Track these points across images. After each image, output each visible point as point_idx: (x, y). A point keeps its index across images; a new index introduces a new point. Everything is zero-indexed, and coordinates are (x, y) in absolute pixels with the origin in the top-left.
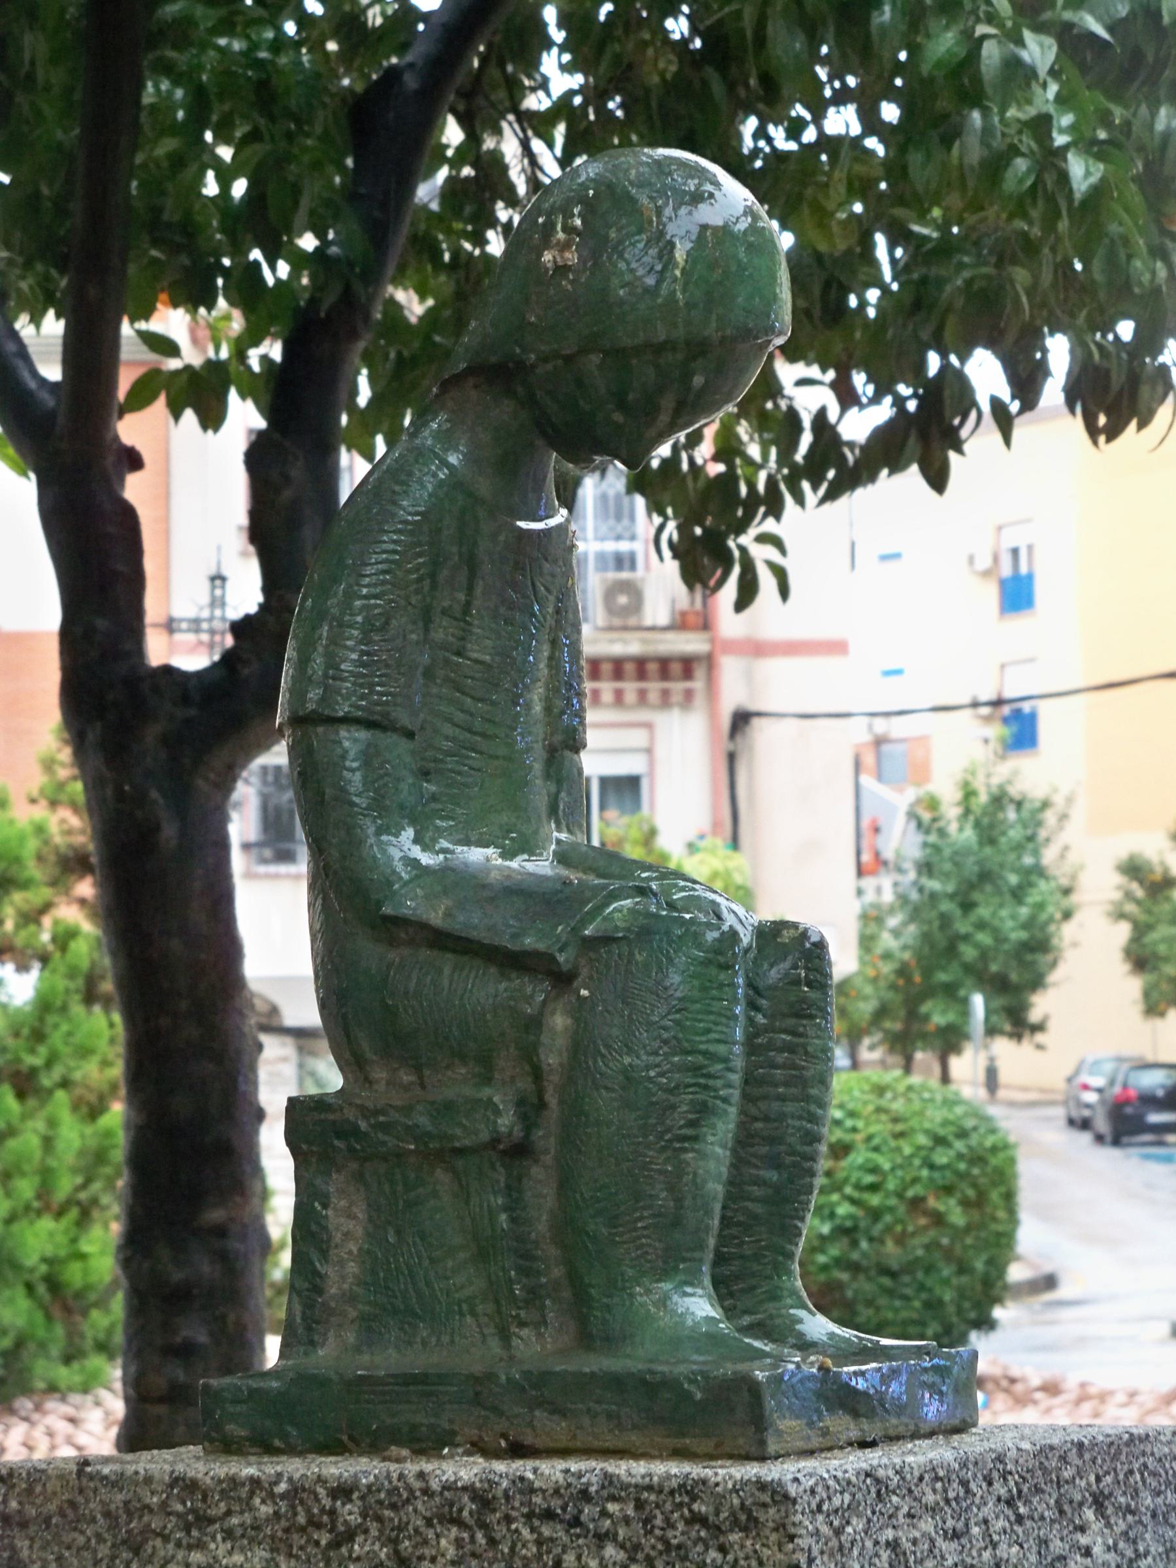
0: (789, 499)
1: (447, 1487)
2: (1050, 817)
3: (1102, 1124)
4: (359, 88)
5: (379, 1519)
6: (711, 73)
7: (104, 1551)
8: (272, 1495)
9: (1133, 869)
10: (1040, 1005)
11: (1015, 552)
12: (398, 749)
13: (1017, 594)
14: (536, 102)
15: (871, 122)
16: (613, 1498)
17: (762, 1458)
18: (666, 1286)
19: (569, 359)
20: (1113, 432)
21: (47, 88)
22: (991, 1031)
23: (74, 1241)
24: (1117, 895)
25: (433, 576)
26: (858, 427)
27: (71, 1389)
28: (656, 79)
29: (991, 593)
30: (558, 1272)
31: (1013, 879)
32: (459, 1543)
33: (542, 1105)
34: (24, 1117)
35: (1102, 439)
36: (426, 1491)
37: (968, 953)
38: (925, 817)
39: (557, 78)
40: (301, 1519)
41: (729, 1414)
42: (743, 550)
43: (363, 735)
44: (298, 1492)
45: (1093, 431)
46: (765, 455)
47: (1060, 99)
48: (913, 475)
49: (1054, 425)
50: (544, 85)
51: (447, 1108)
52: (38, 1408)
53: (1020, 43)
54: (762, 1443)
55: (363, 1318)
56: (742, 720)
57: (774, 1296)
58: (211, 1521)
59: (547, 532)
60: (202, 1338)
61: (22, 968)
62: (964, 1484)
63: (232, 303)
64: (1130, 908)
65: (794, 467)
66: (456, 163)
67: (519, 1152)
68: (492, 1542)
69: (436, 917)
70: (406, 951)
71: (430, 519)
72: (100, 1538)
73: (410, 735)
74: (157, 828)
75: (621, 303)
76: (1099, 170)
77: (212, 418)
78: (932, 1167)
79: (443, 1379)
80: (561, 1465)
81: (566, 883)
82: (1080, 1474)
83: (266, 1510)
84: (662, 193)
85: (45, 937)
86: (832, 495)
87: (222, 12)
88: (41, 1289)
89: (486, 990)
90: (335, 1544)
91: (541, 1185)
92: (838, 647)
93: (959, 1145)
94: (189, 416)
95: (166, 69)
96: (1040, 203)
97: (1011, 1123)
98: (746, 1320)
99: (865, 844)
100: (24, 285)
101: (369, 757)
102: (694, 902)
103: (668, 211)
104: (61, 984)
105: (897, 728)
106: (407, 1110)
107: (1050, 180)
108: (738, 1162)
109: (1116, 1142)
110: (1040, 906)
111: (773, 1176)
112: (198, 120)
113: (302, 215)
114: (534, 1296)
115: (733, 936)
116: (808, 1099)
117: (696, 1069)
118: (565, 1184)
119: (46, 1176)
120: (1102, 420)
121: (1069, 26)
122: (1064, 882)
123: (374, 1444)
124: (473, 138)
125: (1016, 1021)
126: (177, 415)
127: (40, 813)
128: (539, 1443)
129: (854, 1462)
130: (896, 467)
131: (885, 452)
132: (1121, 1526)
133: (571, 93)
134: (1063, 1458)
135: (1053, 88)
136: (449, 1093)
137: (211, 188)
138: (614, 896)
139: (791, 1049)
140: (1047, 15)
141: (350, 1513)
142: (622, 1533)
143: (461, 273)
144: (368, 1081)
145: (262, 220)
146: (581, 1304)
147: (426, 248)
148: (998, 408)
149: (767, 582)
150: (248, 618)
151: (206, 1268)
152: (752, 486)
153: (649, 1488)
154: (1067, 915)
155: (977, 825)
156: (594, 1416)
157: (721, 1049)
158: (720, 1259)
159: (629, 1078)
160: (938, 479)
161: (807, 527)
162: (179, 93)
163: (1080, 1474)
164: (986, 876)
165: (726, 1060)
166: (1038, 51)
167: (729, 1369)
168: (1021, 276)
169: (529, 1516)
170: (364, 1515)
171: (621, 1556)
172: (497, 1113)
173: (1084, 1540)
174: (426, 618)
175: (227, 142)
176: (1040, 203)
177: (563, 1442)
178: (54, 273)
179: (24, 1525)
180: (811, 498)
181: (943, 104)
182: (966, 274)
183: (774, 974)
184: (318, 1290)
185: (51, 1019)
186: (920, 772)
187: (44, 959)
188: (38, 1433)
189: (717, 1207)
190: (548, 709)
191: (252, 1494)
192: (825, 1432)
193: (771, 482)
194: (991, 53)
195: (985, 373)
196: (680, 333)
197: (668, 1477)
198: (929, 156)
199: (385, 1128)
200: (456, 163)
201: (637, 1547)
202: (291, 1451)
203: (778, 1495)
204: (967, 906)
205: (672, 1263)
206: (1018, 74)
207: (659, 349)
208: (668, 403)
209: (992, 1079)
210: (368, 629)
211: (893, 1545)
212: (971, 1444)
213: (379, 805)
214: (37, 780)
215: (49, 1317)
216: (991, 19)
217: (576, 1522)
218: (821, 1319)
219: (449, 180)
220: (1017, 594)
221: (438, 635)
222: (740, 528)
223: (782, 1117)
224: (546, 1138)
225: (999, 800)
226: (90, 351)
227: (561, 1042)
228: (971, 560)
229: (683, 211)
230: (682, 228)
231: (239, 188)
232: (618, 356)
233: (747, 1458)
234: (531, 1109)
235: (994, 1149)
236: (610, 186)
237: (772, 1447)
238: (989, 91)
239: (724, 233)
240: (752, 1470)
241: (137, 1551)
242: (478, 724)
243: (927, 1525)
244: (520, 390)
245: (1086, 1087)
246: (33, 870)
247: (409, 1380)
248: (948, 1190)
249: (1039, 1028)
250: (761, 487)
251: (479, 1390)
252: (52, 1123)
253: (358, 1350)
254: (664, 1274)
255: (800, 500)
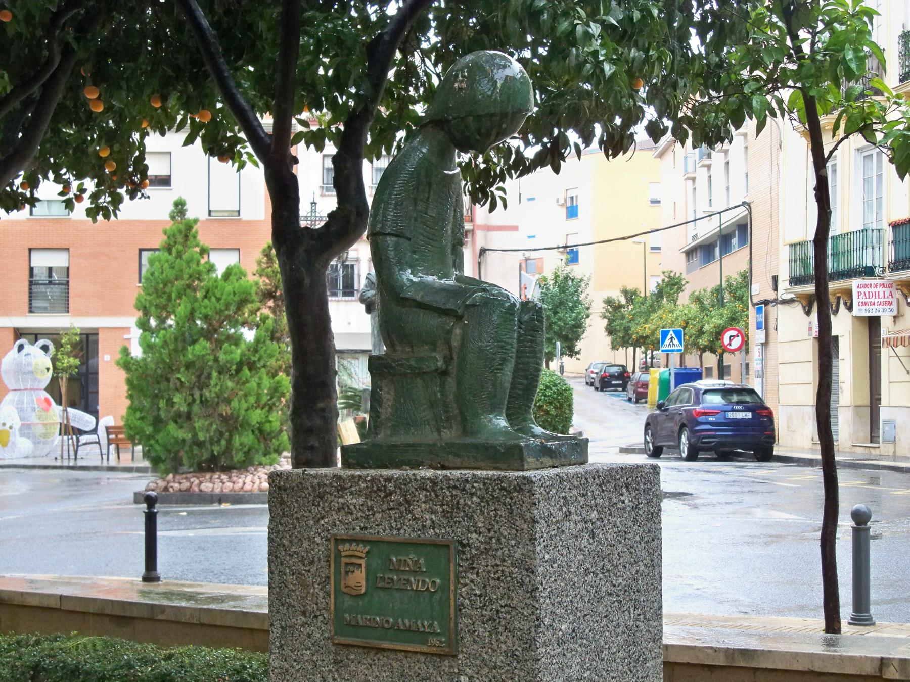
0: (507, 176)
1: (422, 478)
2: (583, 284)
3: (597, 384)
4: (368, 41)
5: (400, 488)
6: (484, 36)
7: (311, 498)
8: (365, 481)
9: (609, 302)
10: (579, 345)
11: (572, 198)
12: (405, 244)
13: (572, 212)
14: (425, 46)
15: (535, 54)
16: (476, 482)
17: (523, 471)
18: (492, 416)
19: (463, 119)
20: (615, 155)
21: (267, 39)
22: (562, 354)
23: (267, 417)
24: (604, 310)
25: (417, 188)
26: (530, 153)
27: (266, 464)
28: (467, 38)
29: (563, 211)
30: (456, 412)
31: (571, 304)
32: (426, 496)
33: (452, 358)
34: (252, 377)
35: (611, 157)
36: (415, 480)
37: (556, 328)
38: (542, 284)
39: (433, 38)
40: (375, 488)
41: (512, 456)
42: (492, 192)
43: (394, 239)
44: (373, 480)
45: (607, 156)
46: (499, 161)
47: (601, 45)
48: (549, 168)
49: (594, 152)
50: (428, 40)
51: (422, 359)
52: (256, 470)
53: (589, 26)
54: (523, 465)
55: (393, 426)
56: (483, 251)
57: (524, 420)
58: (346, 489)
59: (454, 175)
60: (317, 444)
61: (251, 329)
62: (586, 479)
63: (328, 110)
64: (607, 314)
65: (509, 165)
66: (400, 65)
67: (444, 373)
68: (437, 496)
69: (418, 298)
70: (408, 309)
71: (417, 171)
72: (310, 494)
73: (410, 239)
74: (303, 280)
75: (480, 100)
76: (614, 68)
77: (320, 147)
78: (545, 396)
79: (420, 445)
80: (459, 472)
81: (460, 287)
82: (622, 477)
83: (363, 485)
84: (493, 65)
85: (258, 319)
86: (520, 176)
87: (325, 15)
88: (257, 432)
89: (433, 322)
90: (386, 497)
91: (451, 383)
92: (515, 228)
93: (554, 389)
94: (312, 147)
95: (306, 33)
96: (595, 78)
97: (572, 384)
98: (516, 428)
99: (522, 292)
100: (260, 103)
101: (397, 246)
102: (501, 294)
103: (495, 71)
104: (263, 334)
105: (533, 255)
106: (408, 360)
107: (598, 71)
108: (514, 378)
109: (602, 390)
110: (579, 313)
111: (525, 382)
112: (318, 50)
113: (351, 82)
114: (448, 419)
115: (514, 305)
116: (537, 357)
117: (502, 347)
118: (459, 383)
119: (258, 396)
120: (610, 152)
121: (605, 21)
122: (587, 305)
123: (398, 466)
124: (405, 57)
125: (571, 351)
126: (308, 147)
127: (256, 278)
128: (451, 465)
129: (552, 472)
130: (543, 165)
131: (540, 161)
132: (634, 494)
133: (437, 43)
134: (617, 472)
135: (599, 41)
136: (422, 355)
137: (321, 71)
138: (476, 291)
139: (531, 341)
140: (598, 17)
141: (391, 486)
142: (478, 493)
143: (401, 102)
144: (395, 350)
145: (338, 83)
146: (464, 421)
147: (389, 93)
148: (577, 146)
149: (499, 203)
150: (333, 212)
151: (318, 422)
152: (495, 172)
153: (488, 479)
154: (588, 316)
155: (559, 286)
156: (468, 457)
157: (510, 341)
158: (508, 409)
159: (481, 350)
160: (557, 170)
161: (512, 184)
162: (312, 41)
163: (622, 477)
164: (561, 303)
165: (511, 344)
166: (595, 29)
167: (512, 442)
168: (586, 103)
169: (448, 488)
170: (395, 487)
171: (478, 500)
172: (437, 361)
173: (622, 498)
174: (415, 201)
175: (327, 57)
176: (595, 78)
177: (459, 465)
178: (270, 99)
179: (285, 490)
180: (514, 176)
181: (564, 46)
182: (569, 102)
183: (526, 317)
184: (378, 417)
185: (260, 345)
186: (540, 270)
187: (258, 326)
188: (256, 478)
189: (508, 391)
190: (453, 232)
191: (359, 480)
192: (542, 463)
193: (501, 170)
194: (580, 29)
195: (573, 136)
196: (498, 110)
197: (494, 475)
198: (558, 64)
199: (401, 365)
200: (400, 65)
201: (484, 497)
202: (371, 468)
203: (529, 481)
204: (556, 313)
205: (494, 409)
206: (588, 36)
207: (492, 115)
208: (494, 133)
209: (562, 368)
210: (396, 205)
211: (564, 498)
212: (587, 467)
213: (399, 262)
214: (255, 268)
215: (259, 441)
216: (580, 18)
217: (464, 489)
218: (540, 428)
219: (397, 71)
220: (572, 212)
221: (419, 208)
222: (492, 185)
223: (528, 363)
224: (453, 369)
225: (566, 278)
226: (282, 125)
227: (458, 338)
228: (558, 200)
229: (500, 71)
230: (500, 76)
231: (330, 73)
232: (479, 117)
233: (518, 470)
234: (448, 359)
235: (565, 390)
236: (477, 63)
237: (526, 467)
238: (579, 41)
239: (513, 78)
240: (520, 473)
241: (322, 498)
242: (431, 236)
243: (575, 492)
244: (446, 128)
245: (592, 372)
246: (255, 297)
247: (408, 445)
248: (550, 403)
249: (578, 353)
250: (498, 171)
251: (432, 449)
252: (260, 379)
253: (391, 436)
254: (491, 413)
255: (511, 177)
